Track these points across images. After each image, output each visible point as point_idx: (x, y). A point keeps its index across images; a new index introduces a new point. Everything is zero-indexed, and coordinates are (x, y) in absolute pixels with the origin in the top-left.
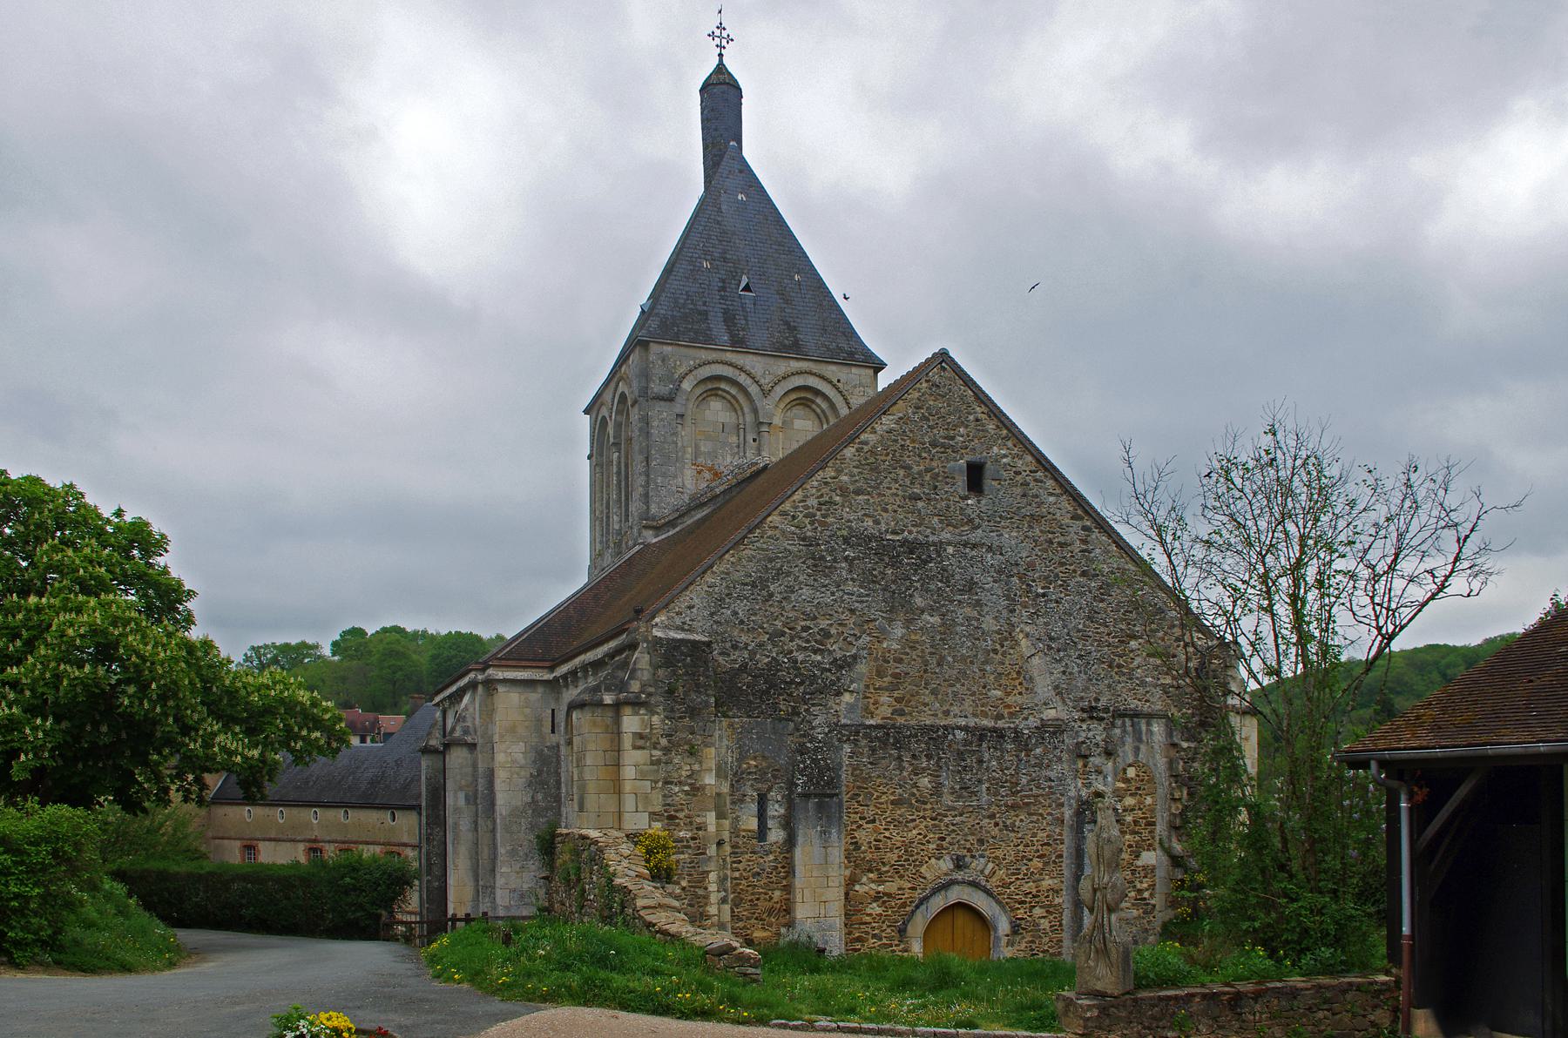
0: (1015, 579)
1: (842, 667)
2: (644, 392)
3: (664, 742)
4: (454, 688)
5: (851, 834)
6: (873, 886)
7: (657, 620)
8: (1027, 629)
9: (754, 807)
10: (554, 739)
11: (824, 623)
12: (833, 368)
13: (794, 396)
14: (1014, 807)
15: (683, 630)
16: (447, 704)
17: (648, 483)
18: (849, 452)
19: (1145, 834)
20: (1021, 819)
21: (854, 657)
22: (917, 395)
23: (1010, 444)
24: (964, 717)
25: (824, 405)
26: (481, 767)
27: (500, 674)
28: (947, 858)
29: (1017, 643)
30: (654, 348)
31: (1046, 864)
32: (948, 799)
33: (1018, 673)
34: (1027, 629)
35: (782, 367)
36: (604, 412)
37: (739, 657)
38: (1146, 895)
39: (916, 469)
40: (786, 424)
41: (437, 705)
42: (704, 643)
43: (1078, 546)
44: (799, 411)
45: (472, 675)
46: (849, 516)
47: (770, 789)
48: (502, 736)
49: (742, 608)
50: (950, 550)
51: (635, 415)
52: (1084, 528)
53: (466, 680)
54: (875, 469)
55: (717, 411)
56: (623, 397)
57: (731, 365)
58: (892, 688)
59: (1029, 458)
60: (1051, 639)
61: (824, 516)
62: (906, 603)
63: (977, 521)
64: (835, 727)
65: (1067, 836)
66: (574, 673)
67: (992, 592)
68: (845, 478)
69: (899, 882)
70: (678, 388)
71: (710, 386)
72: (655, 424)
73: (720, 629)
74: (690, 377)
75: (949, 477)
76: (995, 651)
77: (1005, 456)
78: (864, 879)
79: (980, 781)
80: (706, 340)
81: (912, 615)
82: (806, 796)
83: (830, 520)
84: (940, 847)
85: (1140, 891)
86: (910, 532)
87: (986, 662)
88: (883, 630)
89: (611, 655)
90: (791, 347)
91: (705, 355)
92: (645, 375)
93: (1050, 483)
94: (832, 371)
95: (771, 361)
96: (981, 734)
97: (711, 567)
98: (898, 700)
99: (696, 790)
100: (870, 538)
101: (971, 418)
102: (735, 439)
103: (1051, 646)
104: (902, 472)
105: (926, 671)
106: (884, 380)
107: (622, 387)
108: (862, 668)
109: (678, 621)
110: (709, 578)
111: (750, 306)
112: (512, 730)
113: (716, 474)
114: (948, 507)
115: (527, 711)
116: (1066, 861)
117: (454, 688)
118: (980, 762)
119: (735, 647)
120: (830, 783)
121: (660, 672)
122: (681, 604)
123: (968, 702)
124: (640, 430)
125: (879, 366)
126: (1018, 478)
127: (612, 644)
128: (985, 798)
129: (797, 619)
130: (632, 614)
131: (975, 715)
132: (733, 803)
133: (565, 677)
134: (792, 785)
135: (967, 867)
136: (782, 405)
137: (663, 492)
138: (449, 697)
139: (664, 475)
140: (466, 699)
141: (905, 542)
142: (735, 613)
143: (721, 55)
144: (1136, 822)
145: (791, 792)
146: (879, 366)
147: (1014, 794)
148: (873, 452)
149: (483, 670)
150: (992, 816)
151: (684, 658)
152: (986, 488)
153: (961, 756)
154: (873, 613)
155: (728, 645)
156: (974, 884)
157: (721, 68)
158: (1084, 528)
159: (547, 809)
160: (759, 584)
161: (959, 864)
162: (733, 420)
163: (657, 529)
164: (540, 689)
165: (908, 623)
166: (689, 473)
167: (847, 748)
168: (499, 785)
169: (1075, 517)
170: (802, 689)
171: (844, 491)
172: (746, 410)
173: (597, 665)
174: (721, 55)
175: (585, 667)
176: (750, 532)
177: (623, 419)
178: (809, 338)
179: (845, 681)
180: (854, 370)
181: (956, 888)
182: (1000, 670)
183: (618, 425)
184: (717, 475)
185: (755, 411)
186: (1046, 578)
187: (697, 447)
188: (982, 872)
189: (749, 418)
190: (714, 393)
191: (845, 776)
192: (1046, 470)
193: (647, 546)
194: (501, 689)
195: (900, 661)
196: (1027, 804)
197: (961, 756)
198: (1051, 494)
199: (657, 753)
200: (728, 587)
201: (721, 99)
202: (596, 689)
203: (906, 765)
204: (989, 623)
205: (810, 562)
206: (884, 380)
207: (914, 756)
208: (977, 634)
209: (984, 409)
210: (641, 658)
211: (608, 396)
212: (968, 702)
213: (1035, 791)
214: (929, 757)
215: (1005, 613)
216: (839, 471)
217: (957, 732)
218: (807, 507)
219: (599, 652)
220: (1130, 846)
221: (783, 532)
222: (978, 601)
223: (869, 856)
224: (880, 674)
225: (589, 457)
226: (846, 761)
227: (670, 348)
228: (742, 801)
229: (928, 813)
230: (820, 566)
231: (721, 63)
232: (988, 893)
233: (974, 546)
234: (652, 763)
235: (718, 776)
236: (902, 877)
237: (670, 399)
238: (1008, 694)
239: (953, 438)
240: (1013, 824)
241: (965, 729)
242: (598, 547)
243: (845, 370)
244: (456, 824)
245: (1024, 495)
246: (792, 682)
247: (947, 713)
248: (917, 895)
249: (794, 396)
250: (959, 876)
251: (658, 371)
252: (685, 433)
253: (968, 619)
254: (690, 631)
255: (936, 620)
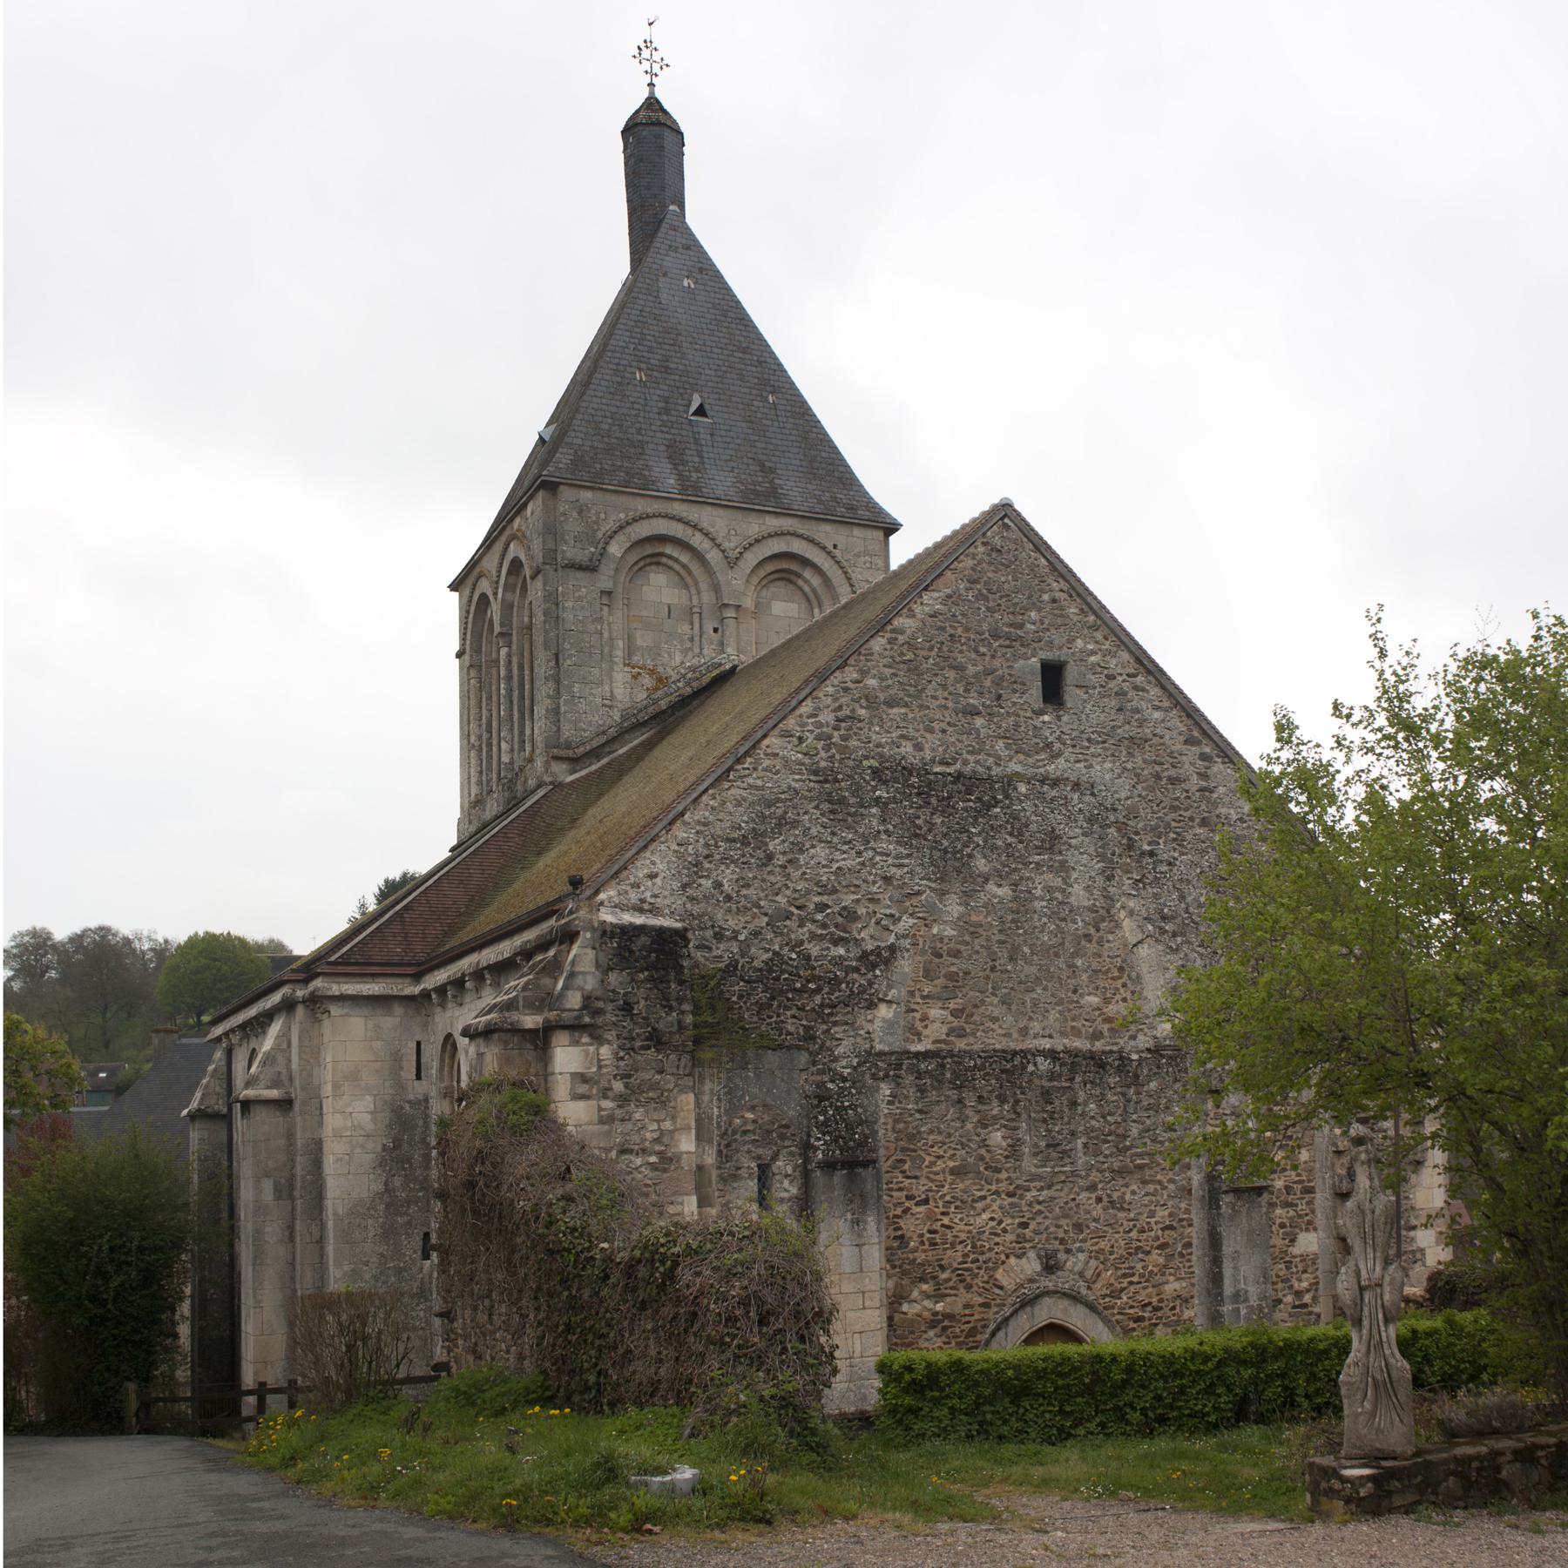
0: (1112, 830)
1: (874, 966)
2: (551, 557)
3: (618, 1086)
4: (252, 1011)
5: (894, 1223)
6: (927, 1303)
7: (602, 896)
8: (1131, 904)
9: (753, 1185)
10: (418, 1089)
11: (848, 899)
12: (827, 527)
13: (770, 567)
14: (1121, 1172)
15: (641, 911)
16: (235, 1039)
17: (558, 691)
18: (878, 644)
19: (1302, 1206)
20: (1132, 1191)
21: (892, 949)
22: (970, 563)
23: (1099, 636)
24: (1046, 1033)
25: (816, 581)
26: (300, 1138)
27: (336, 989)
28: (1032, 1254)
29: (1118, 925)
30: (566, 493)
31: (1170, 1257)
32: (1029, 1164)
33: (1121, 969)
34: (1131, 904)
35: (754, 526)
36: (485, 586)
37: (725, 951)
38: (1307, 1298)
39: (971, 670)
40: (760, 609)
41: (218, 1040)
42: (676, 931)
43: (1195, 782)
44: (779, 588)
45: (285, 990)
46: (890, 737)
47: (775, 1157)
48: (336, 1087)
49: (728, 876)
50: (1022, 788)
51: (536, 590)
52: (1203, 757)
53: (276, 998)
54: (914, 669)
55: (659, 589)
56: (516, 565)
57: (680, 520)
58: (943, 997)
59: (1126, 656)
60: (1164, 918)
61: (845, 738)
62: (964, 867)
63: (1057, 746)
64: (870, 1057)
65: (1197, 1216)
66: (458, 983)
67: (1083, 861)
68: (872, 682)
69: (964, 1296)
70: (603, 552)
71: (649, 550)
72: (570, 604)
73: (696, 909)
74: (620, 537)
75: (1018, 683)
76: (1088, 937)
77: (1092, 653)
78: (915, 1294)
79: (1073, 1133)
80: (640, 484)
81: (971, 886)
82: (829, 1166)
83: (853, 743)
84: (1021, 1239)
85: (1299, 1294)
86: (965, 763)
87: (1076, 954)
88: (931, 908)
89: (527, 953)
90: (760, 497)
91: (641, 506)
92: (551, 531)
93: (1154, 691)
94: (824, 532)
95: (739, 515)
96: (1070, 1062)
97: (682, 814)
98: (956, 1013)
99: (667, 1161)
100: (909, 771)
101: (1046, 597)
102: (686, 627)
103: (1164, 926)
104: (951, 674)
105: (993, 969)
106: (901, 550)
107: (514, 550)
108: (906, 965)
109: (634, 896)
110: (680, 832)
111: (705, 437)
112: (354, 1075)
113: (660, 680)
114: (1017, 725)
115: (378, 1045)
116: (1196, 1252)
117: (252, 1011)
118: (1073, 1104)
119: (719, 936)
120: (862, 1144)
121: (614, 978)
122: (640, 871)
123: (1053, 1015)
124: (546, 613)
125: (891, 528)
126: (1112, 685)
127: (530, 935)
128: (1082, 1159)
129: (808, 892)
130: (568, 888)
131: (1063, 1034)
132: (723, 1179)
133: (441, 990)
134: (807, 1147)
135: (1061, 1268)
136: (755, 580)
137: (582, 706)
138: (243, 1027)
139: (583, 681)
140: (275, 1028)
141: (959, 777)
142: (718, 885)
143: (651, 85)
144: (1288, 1189)
145: (807, 1161)
146: (891, 528)
147: (1121, 1151)
148: (910, 645)
149: (306, 981)
150: (1092, 1187)
151: (652, 954)
152: (1067, 697)
153: (1046, 1095)
154: (918, 883)
155: (709, 933)
156: (1074, 1297)
157: (652, 104)
158: (1203, 757)
159: (408, 1202)
160: (752, 839)
161: (1050, 1266)
162: (685, 601)
163: (575, 762)
164: (399, 1010)
165: (967, 896)
166: (621, 676)
167: (885, 1090)
168: (330, 1165)
169: (1190, 741)
170: (818, 999)
171: (871, 701)
172: (703, 586)
173: (502, 969)
174: (651, 85)
175: (478, 975)
176: (738, 761)
177: (509, 606)
178: (793, 488)
179: (881, 986)
180: (857, 532)
181: (1047, 1301)
182: (1095, 965)
183: (507, 607)
184: (661, 681)
185: (716, 588)
186: (1154, 829)
187: (630, 639)
188: (1081, 1274)
189: (707, 597)
190: (655, 560)
191: (884, 1133)
192: (1149, 672)
193: (558, 786)
194: (335, 1010)
195: (956, 954)
196: (1141, 1167)
197: (1046, 1095)
198: (1157, 708)
199: (607, 1104)
200: (707, 845)
201: (652, 143)
202: (510, 1006)
203: (970, 1112)
204: (1079, 895)
205: (825, 806)
206: (901, 550)
207: (980, 1099)
208: (1061, 911)
209: (1065, 586)
210: (582, 955)
211: (490, 564)
212: (1053, 1015)
213: (1151, 1147)
214: (1002, 1099)
215: (1100, 881)
216: (864, 673)
217: (1040, 1059)
218: (819, 725)
219: (505, 949)
220: (1282, 1226)
221: (786, 761)
222: (1063, 863)
223: (920, 1257)
224: (929, 974)
225: (459, 655)
226: (884, 1109)
227: (588, 495)
228: (735, 1177)
229: (1003, 1186)
230: (839, 809)
231: (652, 93)
232: (1091, 1307)
233: (1055, 783)
234: (601, 1121)
235: (698, 1138)
236: (969, 1287)
237: (591, 568)
238: (1107, 1001)
239: (1021, 626)
240: (1122, 1198)
241: (1052, 1054)
242: (474, 790)
243: (844, 530)
244: (258, 1233)
245: (1120, 710)
246: (804, 990)
247: (1024, 1032)
248: (994, 1315)
249: (770, 567)
250: (1048, 1283)
251: (573, 526)
252: (616, 619)
253: (1049, 890)
254: (654, 911)
255: (1004, 892)
